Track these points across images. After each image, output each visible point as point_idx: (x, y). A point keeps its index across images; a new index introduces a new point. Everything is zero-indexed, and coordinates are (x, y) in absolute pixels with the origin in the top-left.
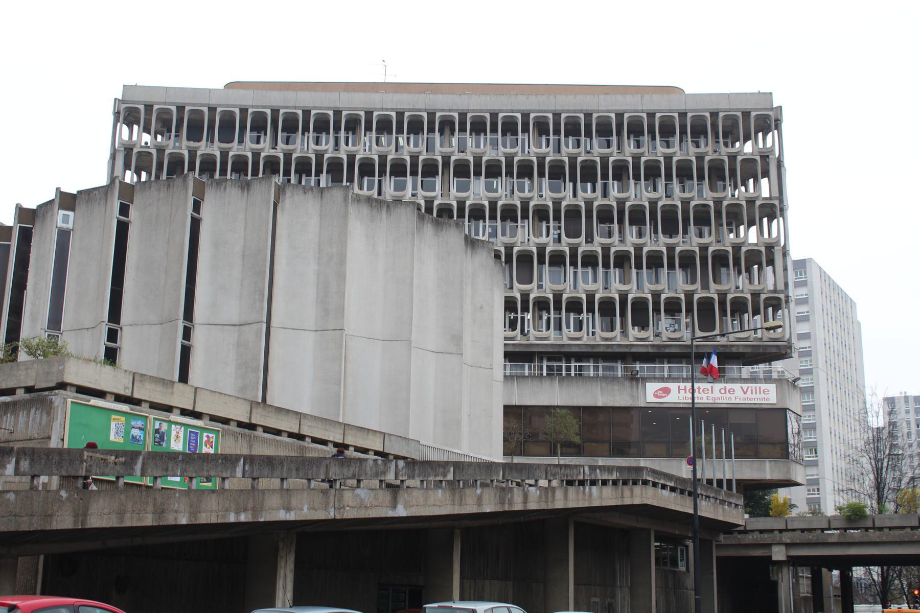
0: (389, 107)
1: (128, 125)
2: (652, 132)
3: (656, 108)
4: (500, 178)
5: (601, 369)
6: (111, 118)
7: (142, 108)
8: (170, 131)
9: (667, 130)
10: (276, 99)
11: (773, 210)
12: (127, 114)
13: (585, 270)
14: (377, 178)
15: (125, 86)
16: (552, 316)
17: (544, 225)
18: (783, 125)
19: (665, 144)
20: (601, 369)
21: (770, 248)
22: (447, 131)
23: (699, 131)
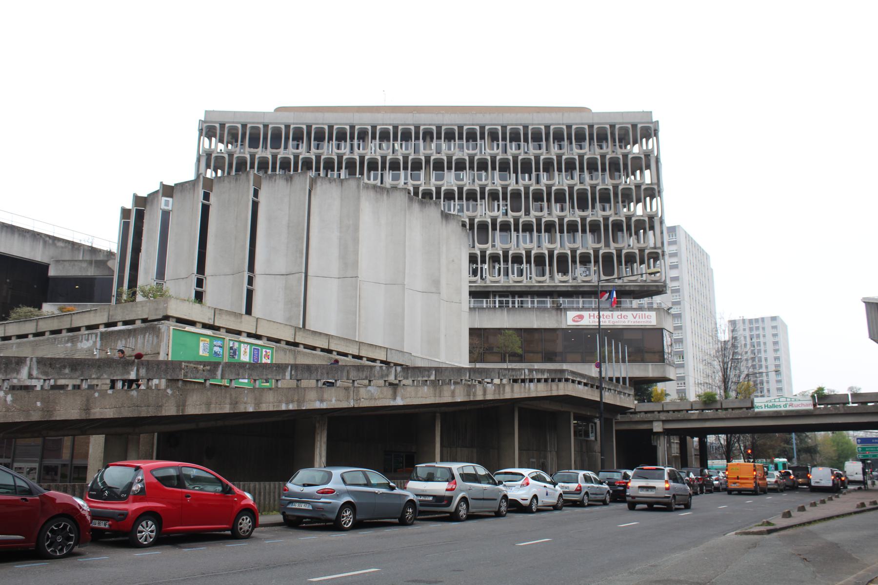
6: (196, 134)
7: (218, 126)
8: (237, 141)
10: (526, 119)
12: (208, 130)
14: (380, 172)
22: (428, 139)
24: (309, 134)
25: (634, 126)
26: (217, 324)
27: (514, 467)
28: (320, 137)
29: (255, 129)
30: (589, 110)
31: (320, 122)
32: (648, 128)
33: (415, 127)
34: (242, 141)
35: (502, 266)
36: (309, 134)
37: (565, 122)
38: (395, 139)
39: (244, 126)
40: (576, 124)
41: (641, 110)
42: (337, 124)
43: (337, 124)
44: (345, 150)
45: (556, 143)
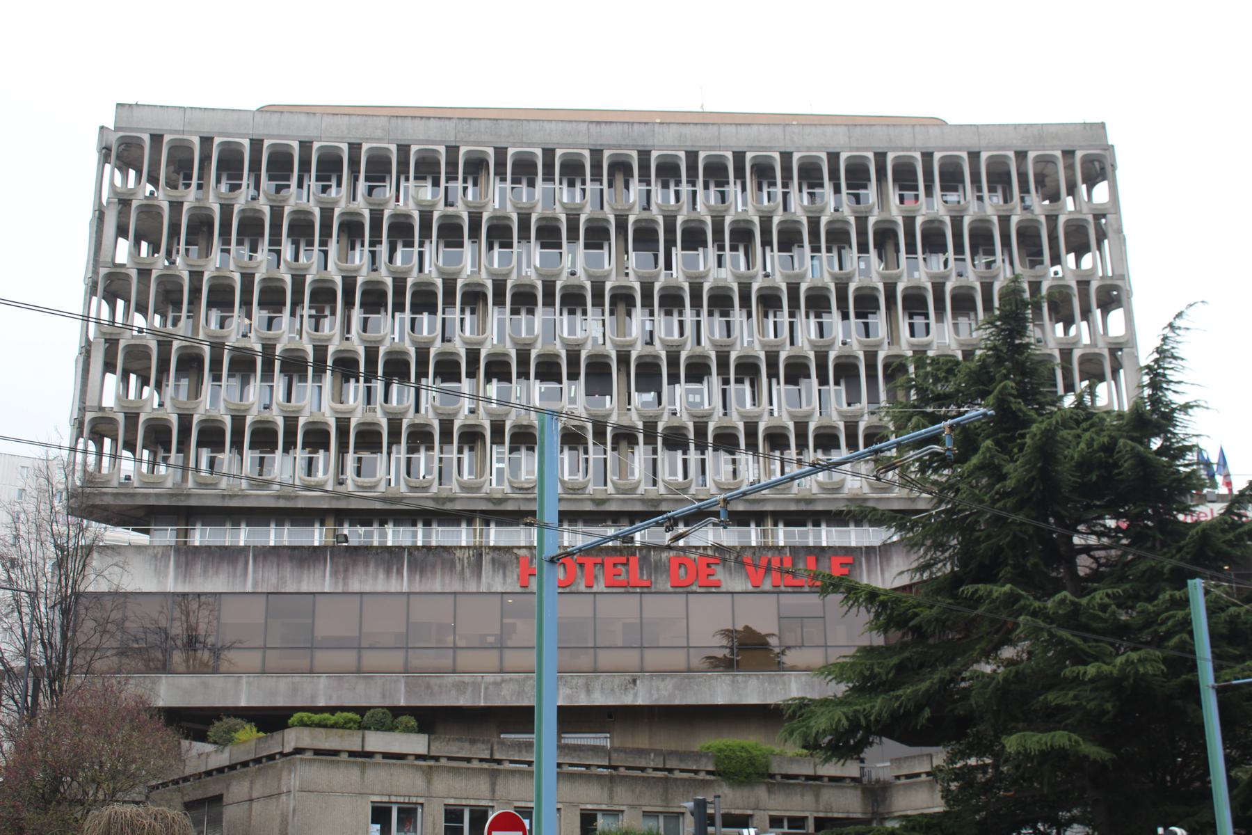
0: (142, 126)
1: (120, 169)
3: (266, 132)
6: (94, 157)
7: (146, 138)
10: (553, 135)
11: (1112, 297)
12: (122, 151)
13: (739, 386)
14: (416, 249)
15: (1103, 125)
16: (591, 456)
17: (676, 318)
19: (853, 199)
21: (1115, 348)
24: (354, 163)
27: (462, 828)
28: (378, 169)
29: (1045, 161)
30: (941, 123)
32: (1099, 159)
37: (919, 144)
38: (452, 177)
39: (206, 141)
42: (752, 149)
44: (339, 196)
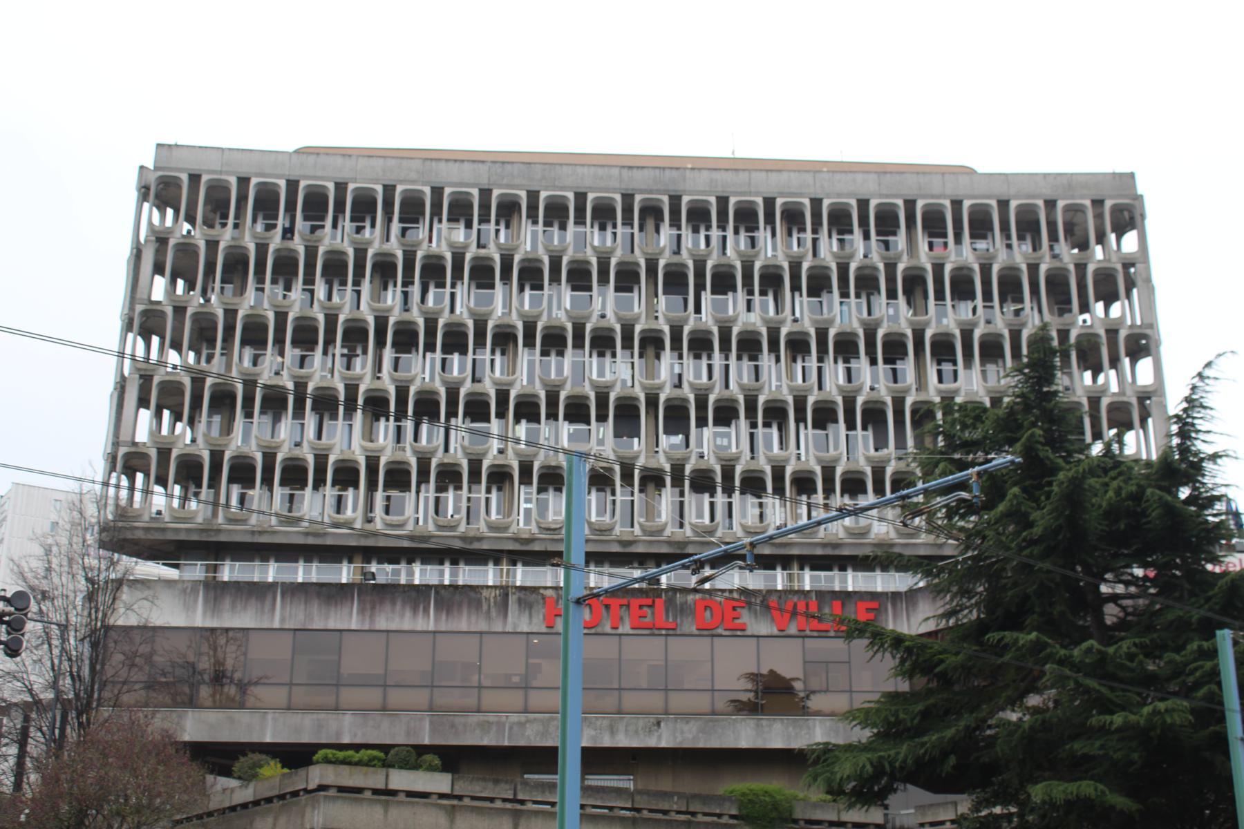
1: (158, 208)
2: (864, 222)
4: (730, 294)
5: (529, 506)
6: (133, 195)
7: (184, 177)
8: (225, 216)
9: (604, 215)
12: (161, 189)
14: (448, 290)
15: (1132, 175)
18: (1147, 222)
20: (529, 506)
21: (1144, 396)
22: (650, 224)
23: (1028, 226)
24: (388, 204)
25: (195, 178)
26: (392, 786)
28: (412, 210)
30: (970, 172)
31: (936, 191)
33: (624, 196)
34: (237, 217)
35: (619, 498)
36: (388, 204)
37: (948, 191)
38: (484, 219)
40: (209, 172)
41: (1110, 171)
43: (594, 190)
44: (373, 236)
45: (835, 237)
